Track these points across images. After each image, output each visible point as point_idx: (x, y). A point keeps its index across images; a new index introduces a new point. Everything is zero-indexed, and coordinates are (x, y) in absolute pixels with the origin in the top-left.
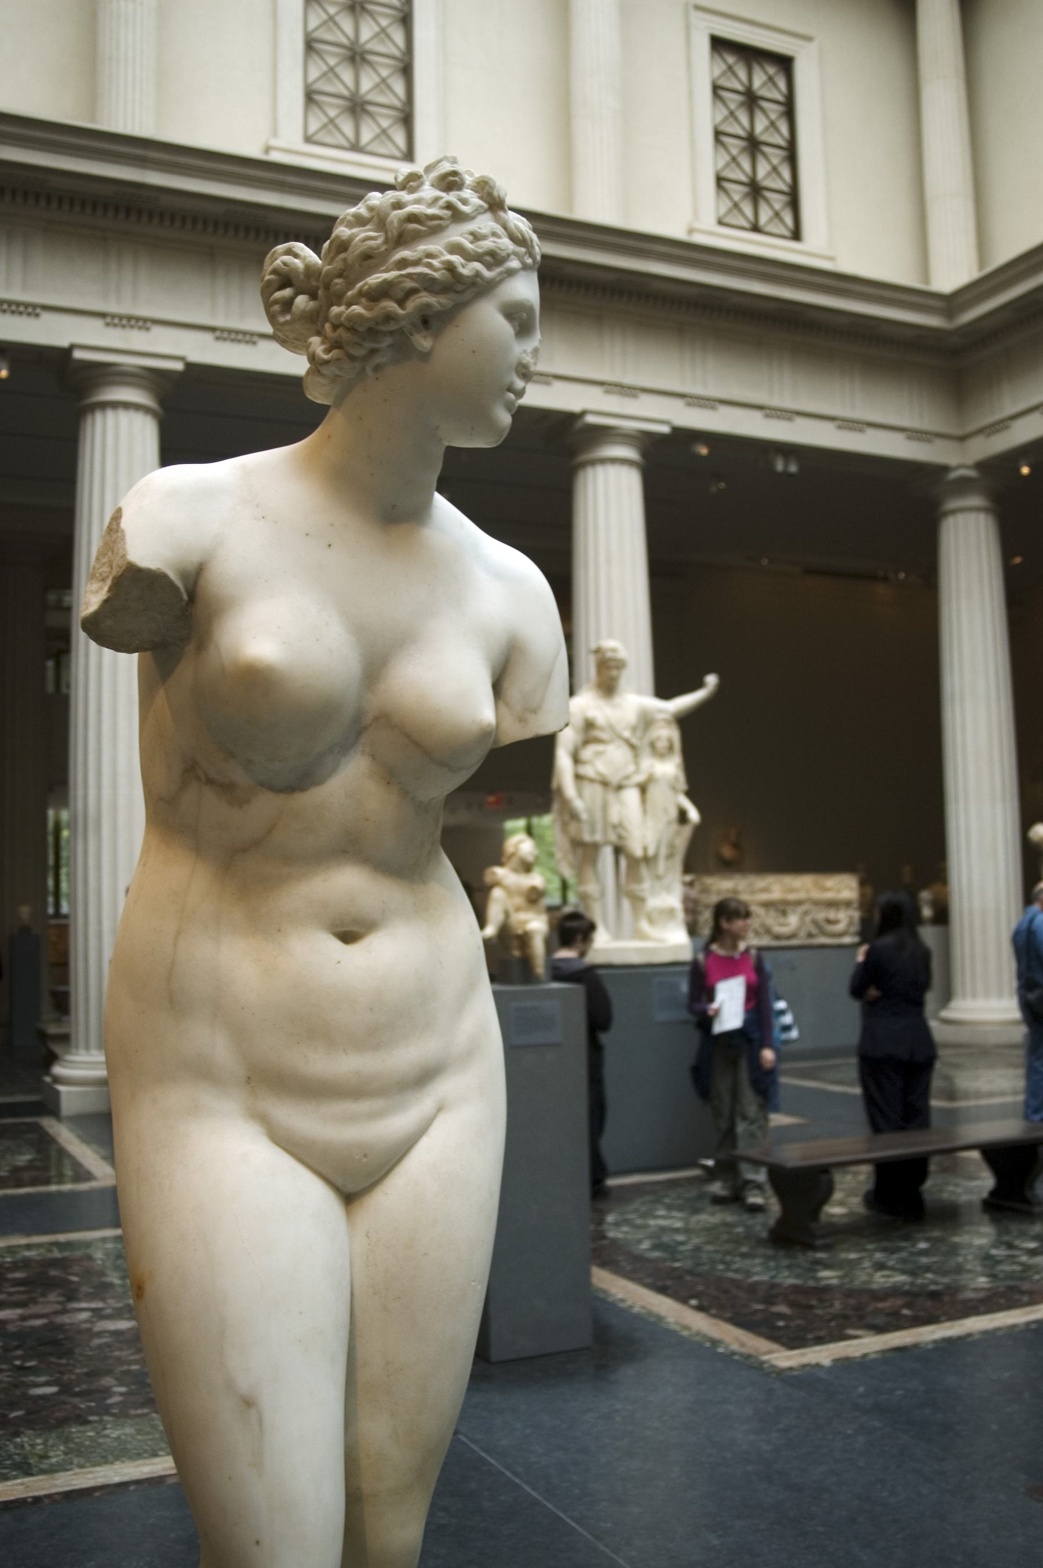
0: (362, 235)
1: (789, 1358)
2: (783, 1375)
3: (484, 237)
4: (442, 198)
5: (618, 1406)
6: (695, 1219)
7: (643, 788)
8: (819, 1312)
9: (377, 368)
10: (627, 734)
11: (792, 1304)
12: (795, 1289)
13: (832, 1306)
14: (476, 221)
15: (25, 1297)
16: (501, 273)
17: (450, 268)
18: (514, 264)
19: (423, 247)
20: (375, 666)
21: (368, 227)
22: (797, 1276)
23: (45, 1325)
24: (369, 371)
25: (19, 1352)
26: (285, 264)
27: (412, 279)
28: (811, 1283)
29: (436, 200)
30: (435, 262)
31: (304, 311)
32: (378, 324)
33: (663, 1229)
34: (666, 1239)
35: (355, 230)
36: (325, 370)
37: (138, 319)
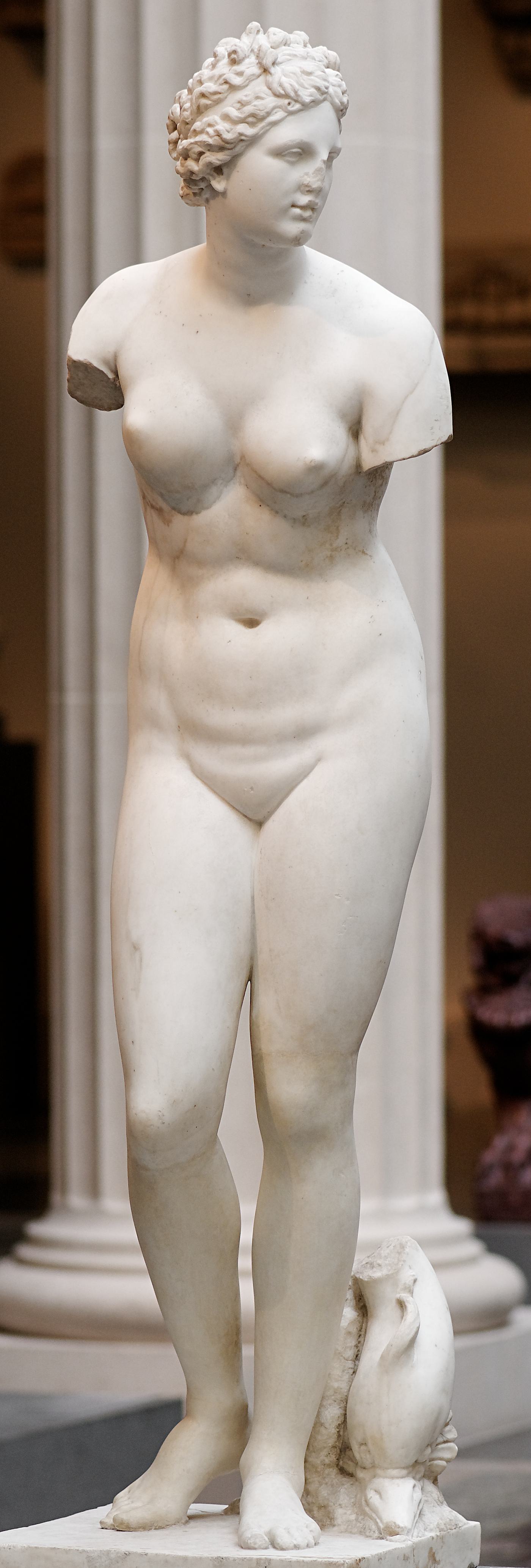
3: (247, 103)
16: (263, 128)
20: (234, 423)
30: (210, 130)
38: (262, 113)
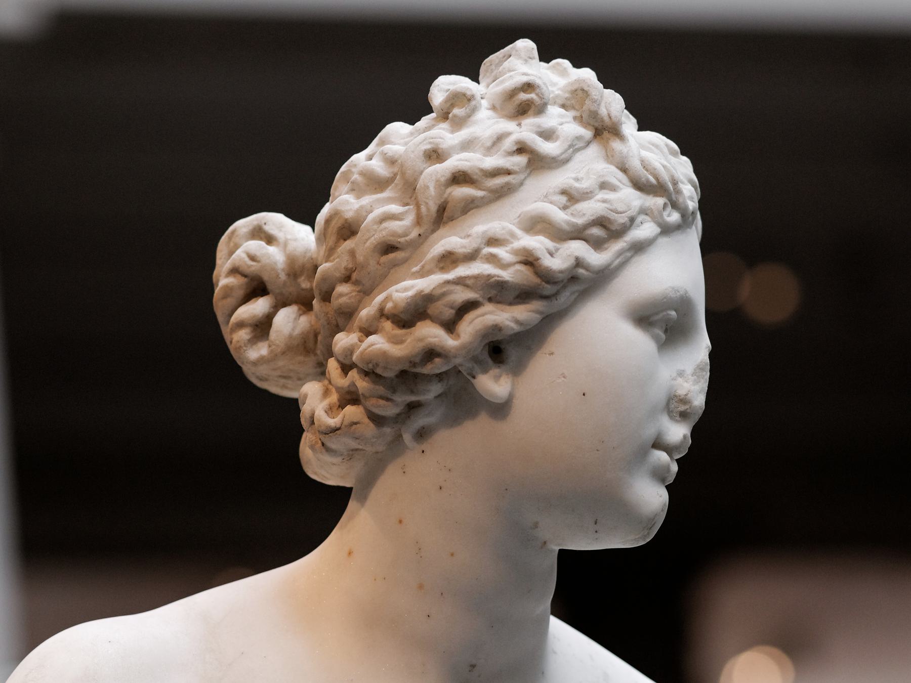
0: (378, 211)
3: (586, 195)
4: (508, 134)
9: (422, 435)
14: (570, 165)
16: (620, 253)
17: (529, 261)
18: (646, 230)
19: (480, 226)
21: (387, 194)
24: (407, 437)
26: (253, 258)
27: (467, 286)
29: (500, 138)
30: (502, 253)
31: (290, 336)
32: (414, 365)
35: (366, 200)
36: (333, 443)
38: (622, 219)
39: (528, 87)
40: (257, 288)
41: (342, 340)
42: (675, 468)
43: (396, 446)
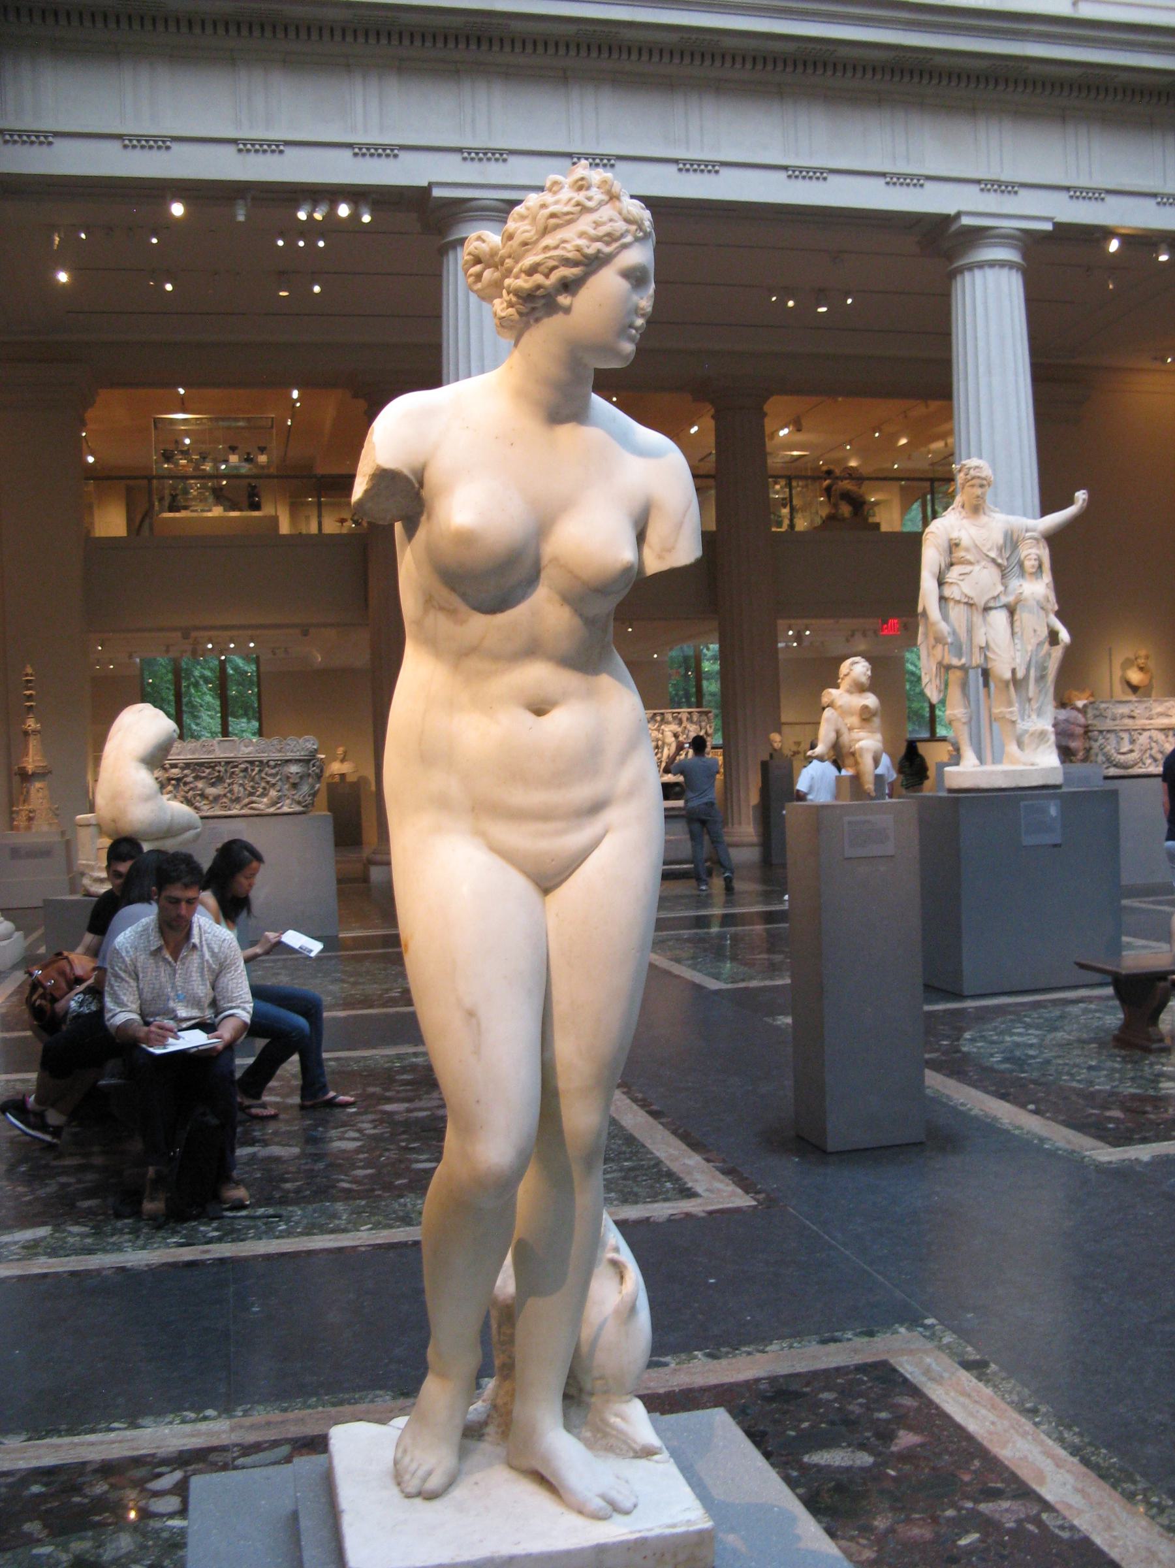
0: (522, 229)
1: (1110, 1154)
2: (1103, 1170)
3: (603, 224)
5: (938, 1189)
6: (1050, 1036)
7: (1011, 610)
8: (1152, 1116)
9: (537, 320)
10: (993, 554)
11: (1126, 1110)
12: (1133, 1097)
13: (1166, 1111)
15: (410, 1094)
20: (542, 529)
21: (526, 222)
22: (1139, 1087)
23: (427, 1116)
24: (532, 321)
25: (405, 1136)
28: (1151, 1092)
29: (570, 200)
33: (1017, 1045)
34: (1018, 1053)
37: (494, 151)
38: (618, 234)
39: (582, 179)
40: (478, 260)
41: (507, 282)
42: (638, 336)
43: (527, 326)
